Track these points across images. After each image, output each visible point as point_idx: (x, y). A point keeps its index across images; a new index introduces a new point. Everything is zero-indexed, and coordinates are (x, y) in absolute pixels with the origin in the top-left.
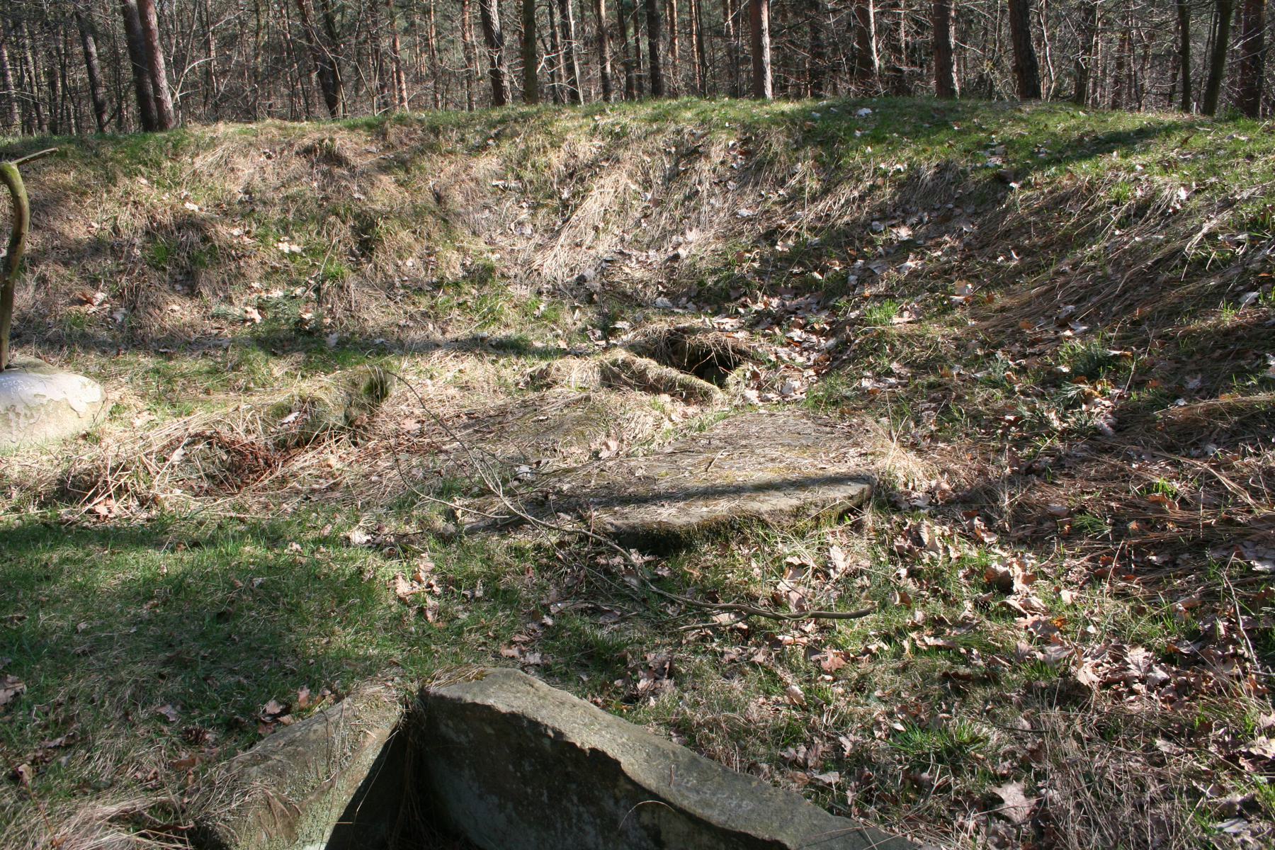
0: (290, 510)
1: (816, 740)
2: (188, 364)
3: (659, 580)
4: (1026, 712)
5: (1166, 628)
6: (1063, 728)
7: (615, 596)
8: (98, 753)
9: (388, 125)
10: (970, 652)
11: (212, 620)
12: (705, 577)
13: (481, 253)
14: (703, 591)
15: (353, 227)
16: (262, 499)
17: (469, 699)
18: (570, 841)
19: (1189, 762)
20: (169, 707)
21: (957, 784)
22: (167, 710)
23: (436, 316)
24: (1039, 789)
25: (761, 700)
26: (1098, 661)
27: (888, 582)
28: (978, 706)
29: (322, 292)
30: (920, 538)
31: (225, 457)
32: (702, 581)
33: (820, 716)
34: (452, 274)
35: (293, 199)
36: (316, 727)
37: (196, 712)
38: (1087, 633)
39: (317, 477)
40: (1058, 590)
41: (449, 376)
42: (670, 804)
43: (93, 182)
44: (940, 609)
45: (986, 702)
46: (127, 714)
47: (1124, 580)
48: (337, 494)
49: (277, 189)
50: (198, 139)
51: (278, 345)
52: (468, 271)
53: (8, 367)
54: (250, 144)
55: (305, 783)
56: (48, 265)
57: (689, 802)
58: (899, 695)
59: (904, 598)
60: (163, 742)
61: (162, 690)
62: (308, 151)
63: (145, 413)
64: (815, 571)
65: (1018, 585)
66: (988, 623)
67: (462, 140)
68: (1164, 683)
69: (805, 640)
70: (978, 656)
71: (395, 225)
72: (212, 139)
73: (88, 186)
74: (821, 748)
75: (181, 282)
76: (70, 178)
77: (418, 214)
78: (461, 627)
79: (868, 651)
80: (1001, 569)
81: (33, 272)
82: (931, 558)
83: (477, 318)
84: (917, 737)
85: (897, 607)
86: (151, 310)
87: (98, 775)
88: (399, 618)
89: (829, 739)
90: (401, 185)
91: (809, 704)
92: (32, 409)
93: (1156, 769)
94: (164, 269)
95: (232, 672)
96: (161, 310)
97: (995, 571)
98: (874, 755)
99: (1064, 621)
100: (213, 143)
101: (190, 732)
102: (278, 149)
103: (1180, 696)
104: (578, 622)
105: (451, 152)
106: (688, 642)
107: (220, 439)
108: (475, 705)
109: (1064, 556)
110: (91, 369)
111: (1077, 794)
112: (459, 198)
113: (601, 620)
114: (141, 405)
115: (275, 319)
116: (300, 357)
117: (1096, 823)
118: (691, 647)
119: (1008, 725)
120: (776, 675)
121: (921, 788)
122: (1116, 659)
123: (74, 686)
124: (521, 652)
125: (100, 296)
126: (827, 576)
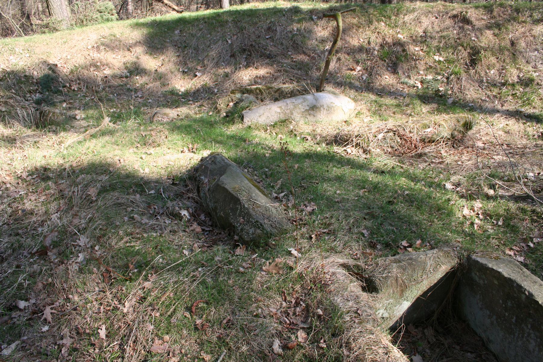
0: (421, 168)
2: (388, 101)
9: (494, 7)
11: (386, 203)
13: (529, 72)
15: (469, 53)
16: (411, 161)
17: (490, 266)
18: (520, 343)
20: (366, 231)
23: (500, 98)
29: (450, 80)
31: (399, 141)
34: (512, 80)
35: (444, 37)
36: (421, 256)
39: (435, 157)
41: (501, 126)
43: (364, 23)
48: (442, 166)
49: (438, 32)
50: (407, 8)
51: (427, 99)
52: (520, 80)
53: (323, 90)
54: (429, 12)
55: (412, 276)
56: (342, 54)
61: (365, 224)
62: (455, 17)
63: (369, 117)
67: (531, 16)
71: (489, 54)
72: (414, 8)
73: (361, 24)
75: (391, 67)
76: (355, 21)
77: (501, 50)
81: (336, 56)
83: (520, 102)
86: (377, 76)
88: (462, 223)
90: (495, 36)
92: (330, 109)
94: (385, 61)
95: (392, 226)
96: (381, 77)
100: (414, 10)
101: (372, 242)
102: (441, 15)
105: (524, 22)
107: (399, 133)
110: (351, 96)
112: (523, 44)
114: (368, 113)
115: (427, 88)
116: (435, 106)
124: (515, 254)
125: (359, 68)
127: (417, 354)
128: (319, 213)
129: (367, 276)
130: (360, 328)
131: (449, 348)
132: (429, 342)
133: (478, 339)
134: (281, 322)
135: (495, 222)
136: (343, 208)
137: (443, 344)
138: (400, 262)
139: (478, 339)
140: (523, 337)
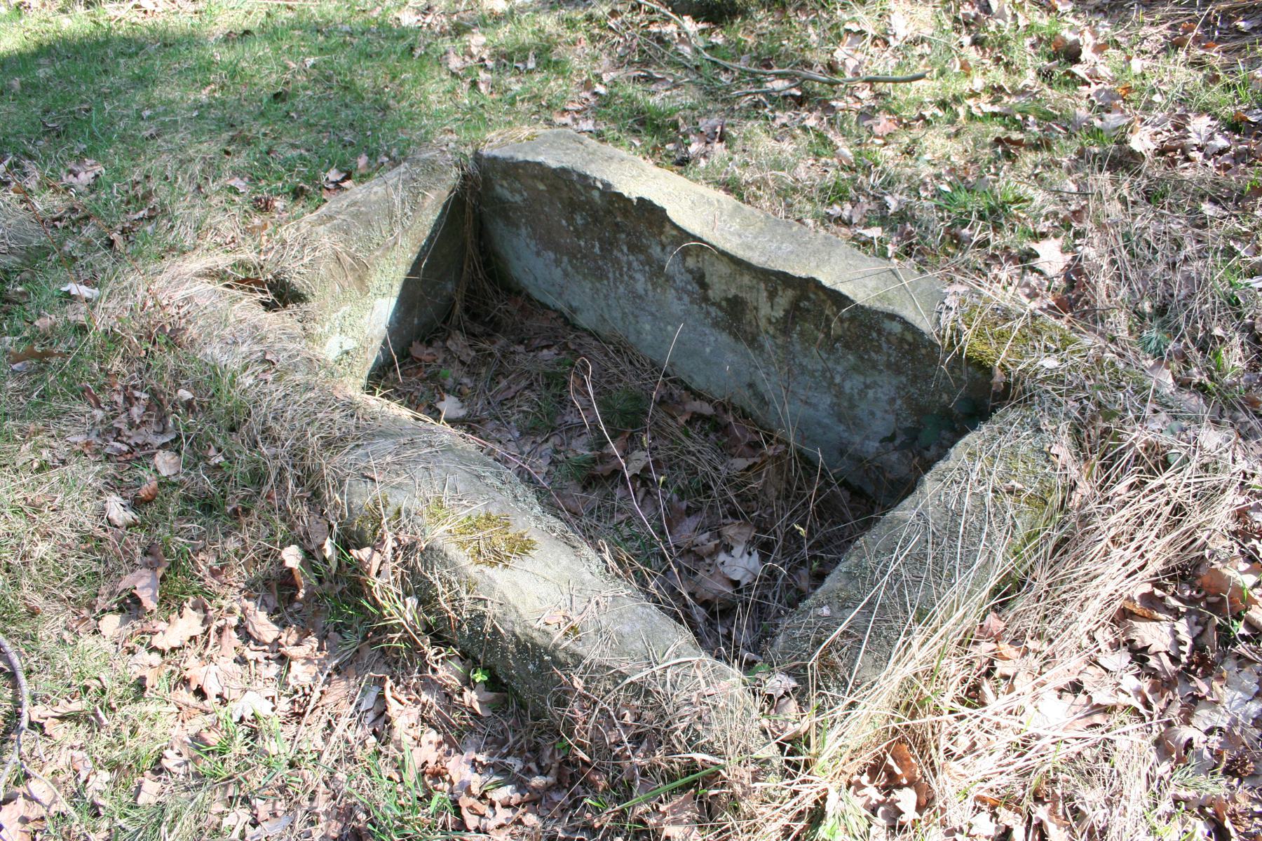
1: (862, 199)
3: (712, 48)
4: (1075, 176)
5: (1238, 96)
6: (1109, 192)
7: (668, 63)
8: (179, 222)
10: (1025, 118)
11: (270, 100)
12: (760, 44)
14: (757, 58)
18: (621, 289)
19: (1233, 224)
21: (996, 240)
22: (237, 182)
24: (1076, 246)
25: (811, 162)
26: (1159, 129)
27: (949, 49)
28: (1027, 170)
30: (989, 6)
32: (757, 48)
33: (868, 176)
36: (375, 189)
37: (264, 183)
38: (1151, 102)
40: (1129, 59)
42: (714, 247)
44: (999, 76)
45: (1036, 166)
46: (199, 187)
47: (1204, 48)
55: (370, 240)
57: (731, 245)
58: (949, 159)
59: (965, 66)
60: (235, 211)
64: (875, 38)
65: (1087, 54)
66: (1049, 91)
68: (1222, 152)
69: (858, 106)
70: (1034, 123)
74: (866, 207)
78: (513, 98)
79: (922, 117)
80: (1071, 37)
82: (998, 26)
84: (962, 196)
85: (956, 75)
87: (182, 241)
89: (875, 198)
91: (858, 166)
93: (1196, 230)
95: (294, 146)
97: (1064, 40)
98: (917, 213)
99: (1129, 90)
103: (1236, 163)
104: (630, 90)
106: (741, 108)
108: (527, 162)
109: (1142, 23)
111: (1113, 252)
113: (653, 87)
117: (1127, 278)
118: (744, 113)
119: (1055, 188)
120: (826, 138)
121: (958, 242)
122: (1177, 128)
123: (148, 166)
124: (574, 120)
126: (886, 43)
127: (446, 396)
128: (114, 180)
129: (270, 277)
130: (281, 388)
131: (503, 356)
132: (463, 363)
133: (554, 316)
134: (108, 457)
135: (521, 65)
136: (166, 146)
137: (491, 355)
138: (331, 218)
139: (554, 316)
140: (621, 275)
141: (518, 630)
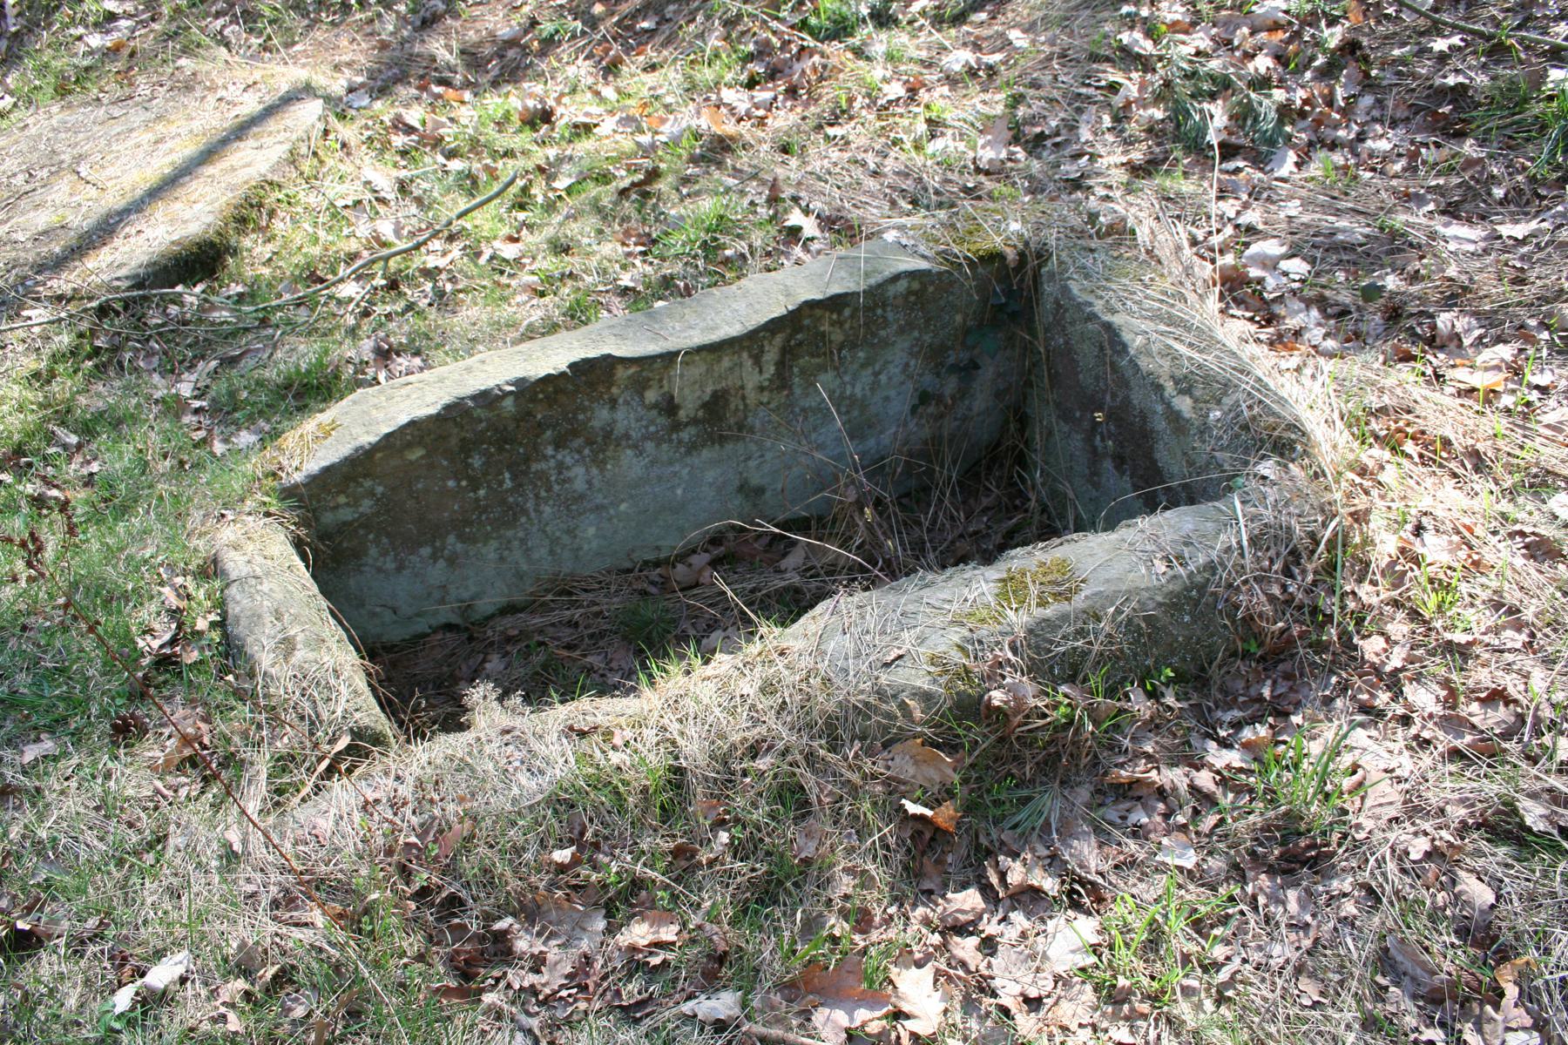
141: (1159, 599)
